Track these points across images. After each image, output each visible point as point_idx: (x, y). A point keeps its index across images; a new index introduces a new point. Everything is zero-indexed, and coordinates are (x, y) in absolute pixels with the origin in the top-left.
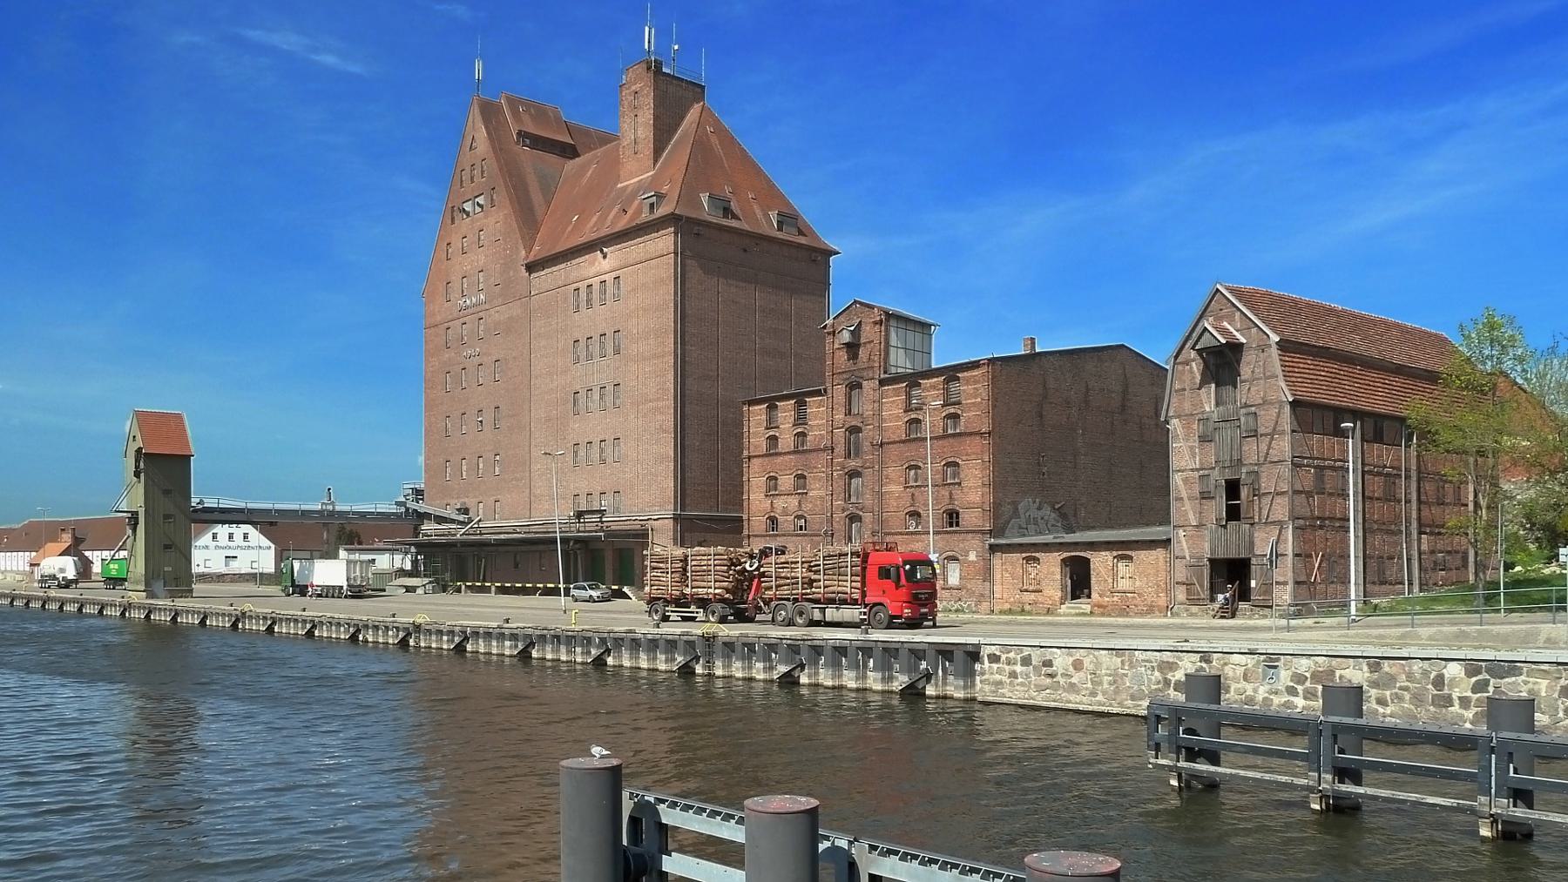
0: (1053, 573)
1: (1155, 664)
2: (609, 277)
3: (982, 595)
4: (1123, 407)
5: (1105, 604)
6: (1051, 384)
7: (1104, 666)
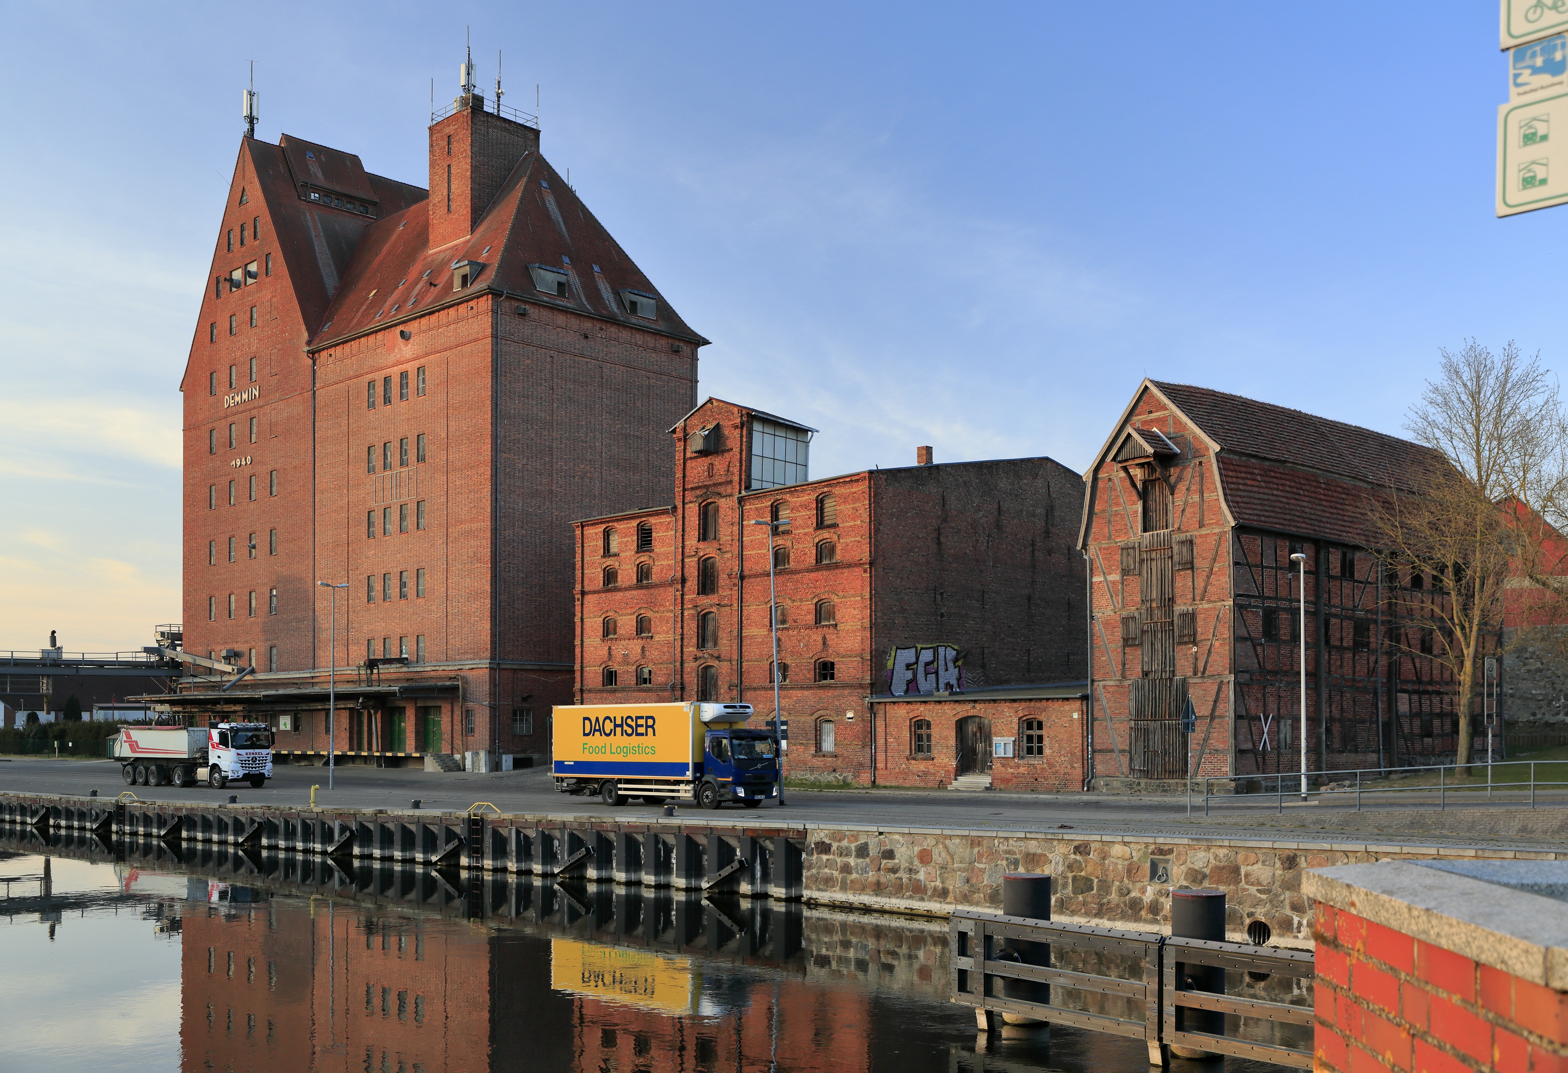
0: (946, 738)
1: (1018, 856)
2: (411, 367)
3: (861, 765)
4: (1047, 533)
5: (1008, 776)
7: (956, 858)
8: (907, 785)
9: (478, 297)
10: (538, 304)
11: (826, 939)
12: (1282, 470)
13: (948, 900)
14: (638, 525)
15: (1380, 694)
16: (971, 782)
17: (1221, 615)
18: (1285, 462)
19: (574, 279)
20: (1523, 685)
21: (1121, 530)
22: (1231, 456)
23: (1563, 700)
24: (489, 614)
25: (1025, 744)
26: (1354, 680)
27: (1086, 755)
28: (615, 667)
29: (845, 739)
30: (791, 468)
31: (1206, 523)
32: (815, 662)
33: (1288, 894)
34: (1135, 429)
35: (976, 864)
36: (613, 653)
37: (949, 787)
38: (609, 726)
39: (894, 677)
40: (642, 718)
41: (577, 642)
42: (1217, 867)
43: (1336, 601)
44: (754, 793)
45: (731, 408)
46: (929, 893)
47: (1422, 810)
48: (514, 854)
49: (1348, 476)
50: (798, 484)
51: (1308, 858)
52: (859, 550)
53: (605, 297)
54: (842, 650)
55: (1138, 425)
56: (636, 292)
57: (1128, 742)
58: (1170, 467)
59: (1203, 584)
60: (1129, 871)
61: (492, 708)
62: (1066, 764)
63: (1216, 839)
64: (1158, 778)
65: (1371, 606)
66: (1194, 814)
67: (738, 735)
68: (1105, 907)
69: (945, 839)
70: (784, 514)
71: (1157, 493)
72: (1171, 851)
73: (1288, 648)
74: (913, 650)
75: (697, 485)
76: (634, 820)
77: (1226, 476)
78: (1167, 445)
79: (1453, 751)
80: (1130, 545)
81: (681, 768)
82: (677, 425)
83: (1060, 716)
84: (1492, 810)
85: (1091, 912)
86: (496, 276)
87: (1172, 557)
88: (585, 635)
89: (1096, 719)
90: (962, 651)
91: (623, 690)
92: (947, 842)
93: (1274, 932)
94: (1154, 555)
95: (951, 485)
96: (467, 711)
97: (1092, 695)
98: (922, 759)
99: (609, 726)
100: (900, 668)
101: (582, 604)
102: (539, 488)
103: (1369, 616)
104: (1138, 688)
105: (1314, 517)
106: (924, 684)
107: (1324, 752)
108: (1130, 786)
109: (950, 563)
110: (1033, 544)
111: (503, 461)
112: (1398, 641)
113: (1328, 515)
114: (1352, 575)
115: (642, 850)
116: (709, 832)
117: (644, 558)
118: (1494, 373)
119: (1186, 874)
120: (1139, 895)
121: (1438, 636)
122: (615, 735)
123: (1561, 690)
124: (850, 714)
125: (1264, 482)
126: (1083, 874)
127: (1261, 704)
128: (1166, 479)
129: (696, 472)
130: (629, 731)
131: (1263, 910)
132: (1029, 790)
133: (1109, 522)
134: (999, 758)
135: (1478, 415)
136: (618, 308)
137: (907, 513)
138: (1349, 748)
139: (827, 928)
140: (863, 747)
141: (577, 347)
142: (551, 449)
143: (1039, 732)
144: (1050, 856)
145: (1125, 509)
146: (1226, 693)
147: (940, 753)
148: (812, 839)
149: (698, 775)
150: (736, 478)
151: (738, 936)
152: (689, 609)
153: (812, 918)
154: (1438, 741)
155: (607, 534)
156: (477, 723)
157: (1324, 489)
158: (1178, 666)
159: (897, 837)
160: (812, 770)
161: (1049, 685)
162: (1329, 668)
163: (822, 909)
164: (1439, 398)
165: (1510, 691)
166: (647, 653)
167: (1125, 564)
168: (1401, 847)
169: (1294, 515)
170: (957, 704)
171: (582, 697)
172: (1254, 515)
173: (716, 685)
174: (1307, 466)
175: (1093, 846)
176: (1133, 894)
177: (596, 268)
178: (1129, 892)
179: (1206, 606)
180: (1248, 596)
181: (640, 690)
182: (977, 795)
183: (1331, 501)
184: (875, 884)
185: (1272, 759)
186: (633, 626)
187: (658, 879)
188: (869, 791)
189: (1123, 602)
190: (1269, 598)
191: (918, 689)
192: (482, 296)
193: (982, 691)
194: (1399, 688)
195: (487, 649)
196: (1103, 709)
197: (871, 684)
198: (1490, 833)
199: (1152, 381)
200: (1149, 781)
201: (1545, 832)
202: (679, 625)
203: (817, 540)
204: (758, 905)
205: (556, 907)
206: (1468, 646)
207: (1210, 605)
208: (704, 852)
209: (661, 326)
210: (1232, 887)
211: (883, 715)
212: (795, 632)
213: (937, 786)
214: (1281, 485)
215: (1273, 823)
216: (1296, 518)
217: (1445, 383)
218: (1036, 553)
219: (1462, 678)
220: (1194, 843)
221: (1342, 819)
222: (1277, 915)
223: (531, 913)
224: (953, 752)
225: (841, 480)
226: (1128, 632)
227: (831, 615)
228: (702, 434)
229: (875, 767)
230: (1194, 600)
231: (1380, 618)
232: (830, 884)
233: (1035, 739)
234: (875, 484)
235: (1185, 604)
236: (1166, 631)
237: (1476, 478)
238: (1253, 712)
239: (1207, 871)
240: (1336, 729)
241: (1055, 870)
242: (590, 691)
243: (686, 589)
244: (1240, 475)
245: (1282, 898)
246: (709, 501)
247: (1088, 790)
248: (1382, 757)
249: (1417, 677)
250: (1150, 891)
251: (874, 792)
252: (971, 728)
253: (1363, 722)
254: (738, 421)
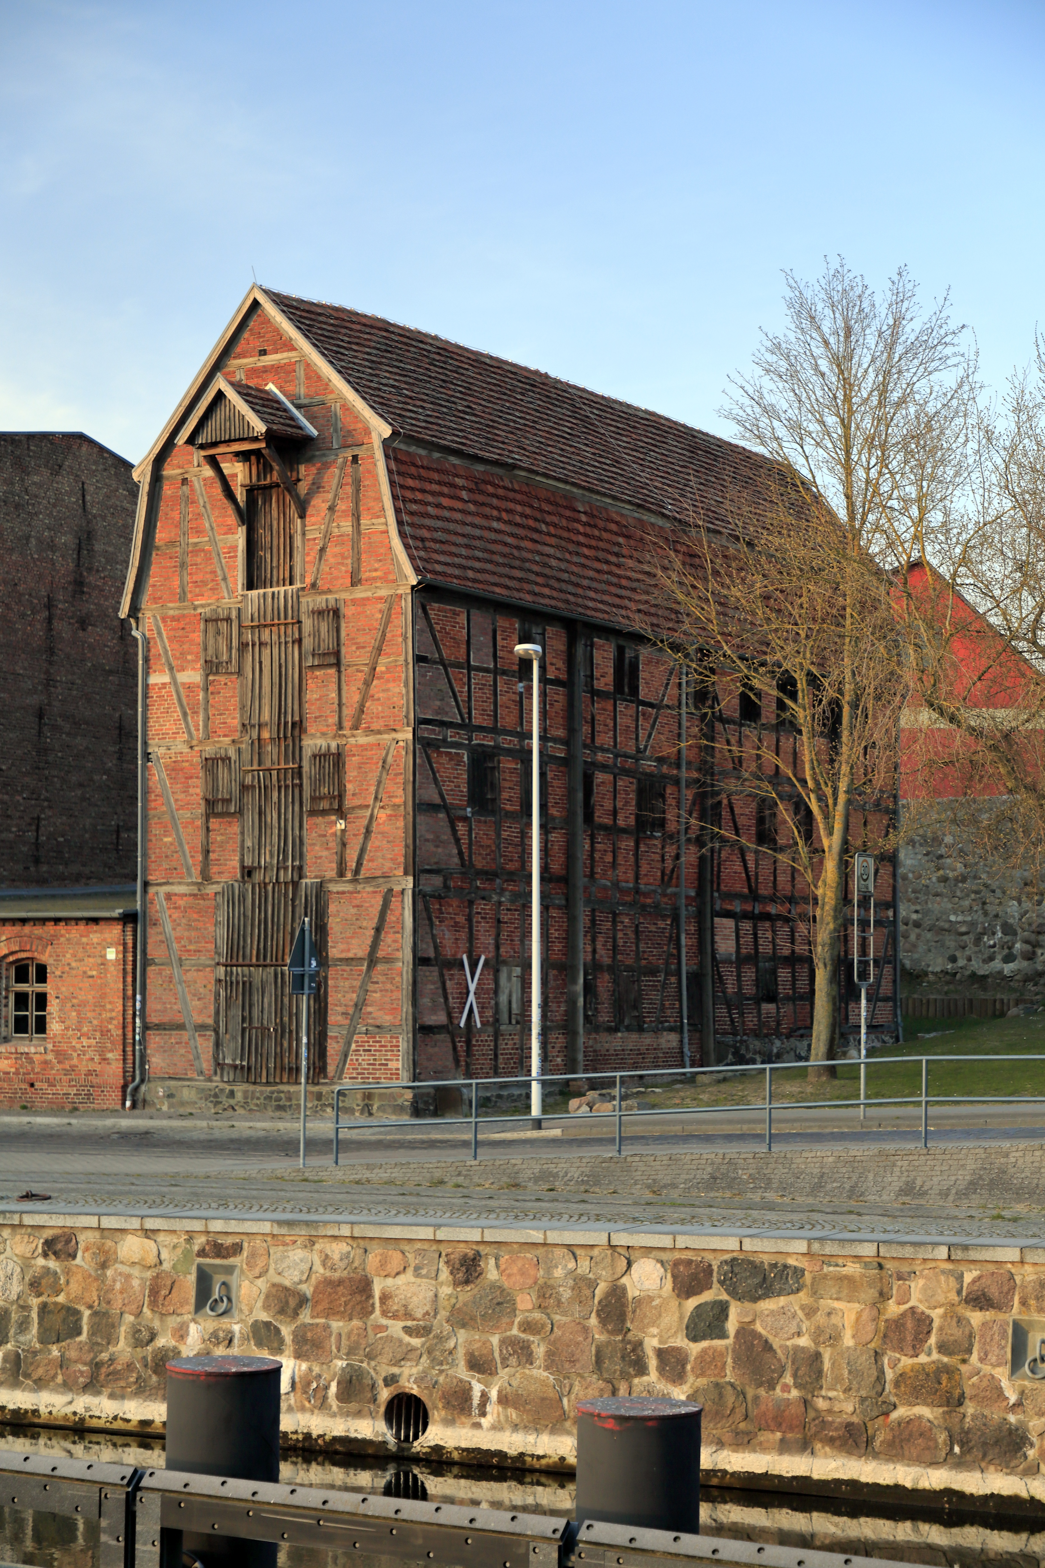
4: (79, 585)
15: (683, 919)
17: (390, 759)
18: (514, 467)
20: (937, 906)
21: (204, 583)
22: (413, 449)
23: (1000, 934)
26: (637, 891)
27: (130, 1035)
31: (364, 576)
33: (462, 1335)
34: (232, 384)
42: (328, 1282)
43: (604, 739)
47: (732, 1150)
49: (629, 502)
51: (502, 1261)
55: (240, 376)
57: (212, 1009)
58: (299, 463)
59: (357, 697)
60: (154, 1292)
62: (90, 1054)
63: (326, 1223)
64: (268, 1083)
65: (668, 751)
68: (103, 1370)
71: (275, 513)
72: (237, 1249)
77: (401, 486)
78: (292, 418)
80: (222, 614)
83: (80, 954)
85: (76, 1382)
87: (300, 641)
89: (153, 962)
93: (435, 1415)
94: (266, 635)
97: (144, 912)
103: (665, 769)
104: (233, 899)
105: (565, 576)
107: (581, 1030)
108: (215, 1098)
110: (50, 605)
112: (717, 820)
113: (591, 574)
114: (635, 690)
118: (875, 324)
119: (267, 1297)
120: (173, 1343)
121: (785, 813)
125: (475, 503)
126: (61, 1299)
127: (464, 935)
128: (291, 486)
131: (414, 1371)
132: (17, 1107)
133: (183, 565)
135: (847, 399)
138: (626, 1022)
143: (39, 988)
145: (213, 541)
146: (397, 913)
157: (585, 524)
158: (309, 858)
161: (79, 889)
164: (782, 363)
165: (914, 916)
167: (210, 651)
168: (674, 1234)
169: (530, 571)
172: (453, 565)
175: (83, 1238)
176: (161, 1342)
178: (153, 1337)
179: (363, 740)
180: (442, 724)
183: (597, 548)
185: (483, 1043)
189: (206, 726)
190: (481, 729)
194: (717, 907)
196: (166, 942)
198: (850, 1198)
200: (251, 1088)
206: (830, 833)
207: (371, 739)
215: (460, 1180)
216: (533, 577)
217: (792, 336)
218: (56, 623)
219: (819, 892)
220: (284, 1231)
221: (587, 1170)
222: (441, 1379)
226: (215, 789)
230: (340, 727)
231: (684, 774)
233: (32, 1002)
235: (324, 734)
236: (287, 787)
238: (448, 952)
239: (307, 1289)
240: (604, 983)
244: (428, 487)
245: (451, 1344)
247: (134, 1106)
248: (686, 1040)
250: (195, 1332)
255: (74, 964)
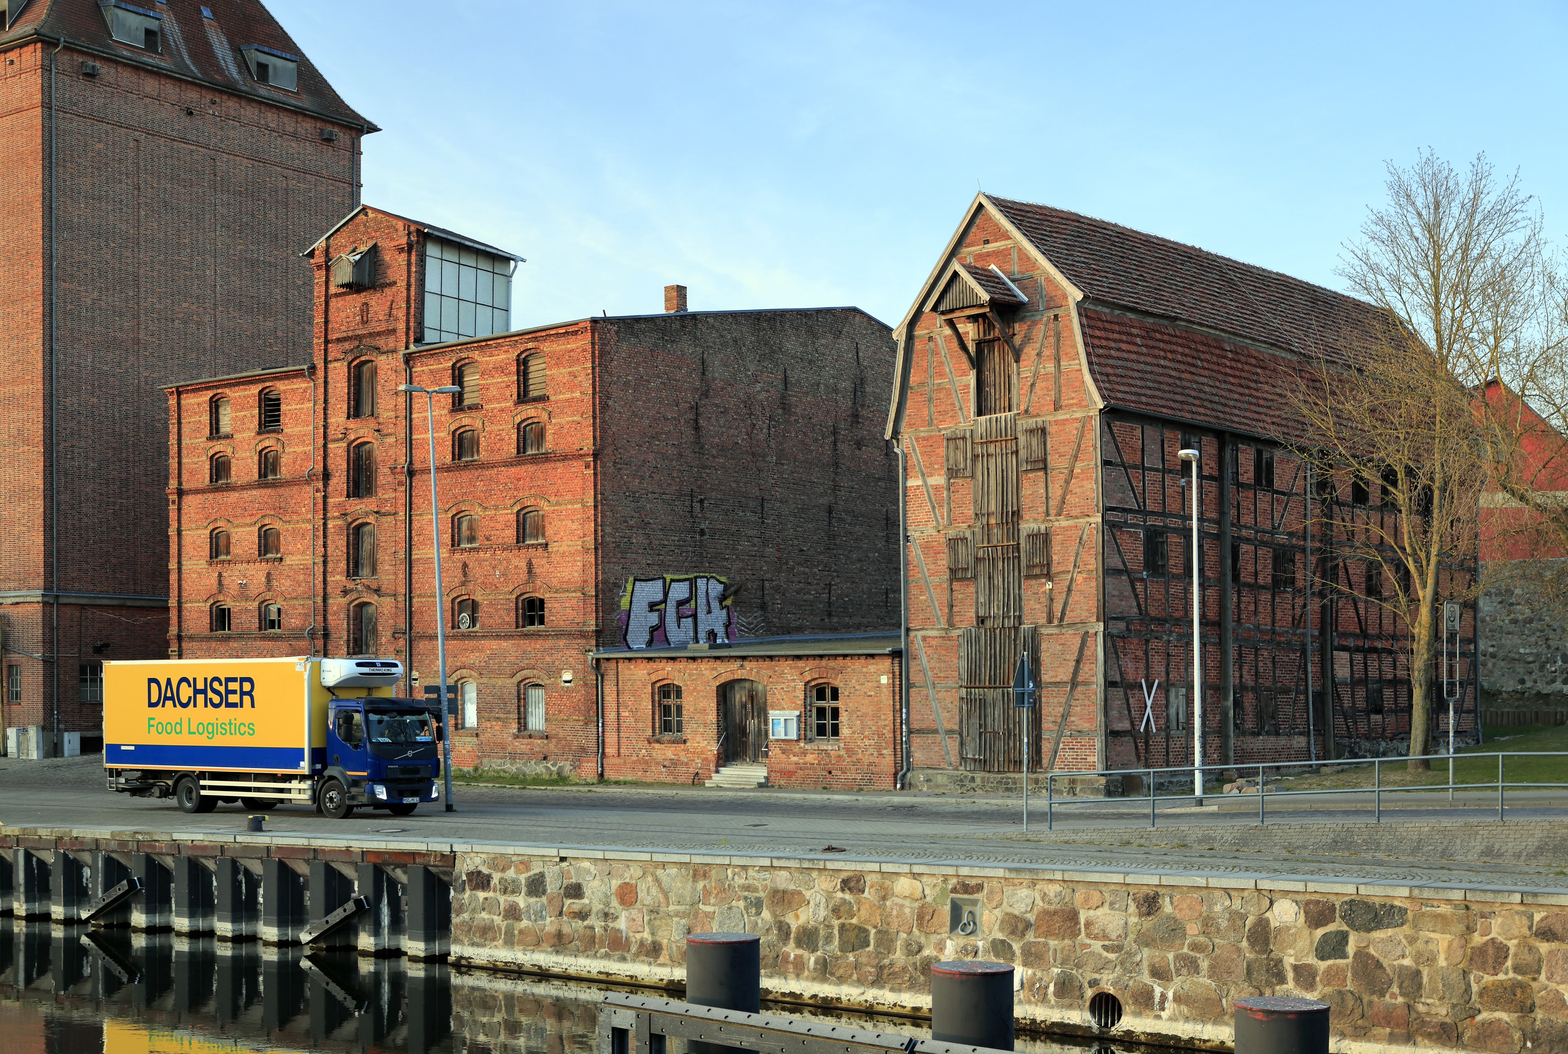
1: (761, 894)
3: (583, 750)
5: (791, 768)
6: (718, 371)
7: (673, 898)
8: (649, 780)
9: (21, 46)
10: (114, 61)
11: (485, 1020)
12: (1171, 331)
13: (661, 960)
14: (260, 392)
15: (1309, 652)
16: (738, 776)
17: (1085, 537)
18: (1176, 319)
19: (171, 26)
20: (1508, 642)
21: (946, 412)
22: (1099, 308)
23: (1560, 663)
24: (41, 522)
25: (814, 721)
27: (898, 737)
28: (229, 604)
29: (560, 712)
30: (484, 314)
31: (1064, 403)
32: (517, 598)
33: (1146, 952)
34: (964, 266)
35: (701, 906)
36: (225, 582)
37: (708, 783)
38: (186, 692)
39: (631, 623)
40: (234, 680)
41: (173, 565)
42: (1046, 912)
43: (1247, 519)
44: (402, 794)
45: (394, 222)
46: (634, 949)
47: (1349, 822)
48: (22, 889)
49: (1265, 342)
50: (495, 335)
51: (1175, 899)
52: (579, 435)
53: (220, 56)
54: (555, 582)
55: (970, 260)
56: (266, 49)
58: (1014, 322)
59: (1060, 492)
60: (920, 917)
61: (48, 663)
62: (871, 751)
63: (1044, 870)
65: (1297, 527)
66: (1035, 827)
67: (377, 707)
68: (886, 971)
69: (656, 868)
70: (471, 379)
71: (997, 360)
72: (979, 888)
73: (1180, 586)
74: (660, 583)
75: (345, 335)
76: (200, 837)
77: (1091, 336)
78: (1009, 290)
79: (1404, 734)
81: (292, 756)
82: (315, 245)
83: (862, 680)
84: (1446, 822)
86: (49, 15)
87: (1017, 452)
88: (183, 555)
90: (732, 585)
91: (240, 637)
92: (659, 872)
93: (1127, 1009)
95: (714, 343)
96: (10, 667)
97: (907, 650)
98: (670, 742)
99: (186, 692)
100: (640, 609)
101: (179, 510)
102: (118, 334)
103: (1294, 541)
104: (971, 640)
105: (1216, 399)
106: (676, 633)
108: (961, 782)
109: (714, 457)
110: (835, 433)
111: (61, 293)
112: (1335, 578)
113: (1236, 396)
114: (1270, 482)
115: (215, 884)
116: (311, 856)
117: (269, 441)
118: (1459, 199)
119: (1002, 922)
121: (1388, 572)
122: (195, 706)
123: (1557, 649)
124: (567, 676)
125: (1146, 346)
126: (854, 921)
127: (1142, 665)
128: (1008, 339)
129: (343, 315)
130: (216, 699)
131: (1111, 977)
132: (820, 788)
133: (930, 399)
134: (777, 740)
135: (1436, 257)
136: (240, 73)
137: (648, 381)
138: (1266, 728)
139: (486, 1002)
140: (586, 724)
141: (176, 127)
142: (136, 279)
143: (833, 704)
144: (807, 894)
146: (1092, 649)
147: (696, 732)
148: (463, 868)
149: (319, 766)
150: (401, 326)
151: (357, 1014)
152: (334, 518)
153: (463, 987)
154: (1391, 719)
155: (215, 406)
156: (25, 685)
157: (1231, 360)
158: (1026, 609)
159: (586, 864)
160: (513, 756)
161: (859, 634)
162: (1239, 615)
163: (478, 973)
166: (275, 583)
167: (951, 461)
168: (1306, 882)
170: (718, 662)
171: (180, 647)
172: (1131, 393)
173: (375, 631)
174: (1208, 326)
175: (869, 879)
177: (206, 12)
180: (1124, 510)
181: (264, 638)
182: (745, 794)
183: (1240, 377)
184: (555, 936)
186: (253, 543)
187: (237, 927)
188: (593, 789)
189: (949, 516)
190: (1153, 513)
191: (667, 640)
192: (26, 44)
193: (761, 643)
194: (1336, 643)
195: (38, 575)
196: (923, 671)
197: (596, 631)
199: (988, 197)
200: (987, 775)
201: (1517, 856)
202: (321, 542)
203: (518, 420)
204: (386, 967)
205: (87, 971)
206: (1424, 587)
207: (1071, 523)
208: (305, 886)
209: (305, 102)
210: (1067, 942)
211: (614, 678)
212: (488, 555)
213: (690, 781)
214: (1170, 351)
215: (1143, 841)
216: (1191, 400)
217: (1392, 211)
219: (1416, 631)
220: (1013, 875)
222: (1131, 983)
223: (48, 982)
224: (712, 731)
225: (552, 332)
227: (539, 530)
228: (351, 259)
229: (603, 753)
230: (1048, 514)
232: (490, 935)
234: (600, 339)
235: (1035, 520)
236: (1009, 558)
237: (1433, 345)
238: (1131, 677)
239: (1031, 917)
240: (1249, 700)
241: (814, 914)
242: (191, 638)
243: (330, 489)
244: (1111, 336)
246: (363, 358)
247: (902, 788)
248: (1312, 742)
249: (1361, 628)
251: (601, 790)
252: (739, 696)
253: (1287, 691)
254: (404, 240)
255: (857, 687)
